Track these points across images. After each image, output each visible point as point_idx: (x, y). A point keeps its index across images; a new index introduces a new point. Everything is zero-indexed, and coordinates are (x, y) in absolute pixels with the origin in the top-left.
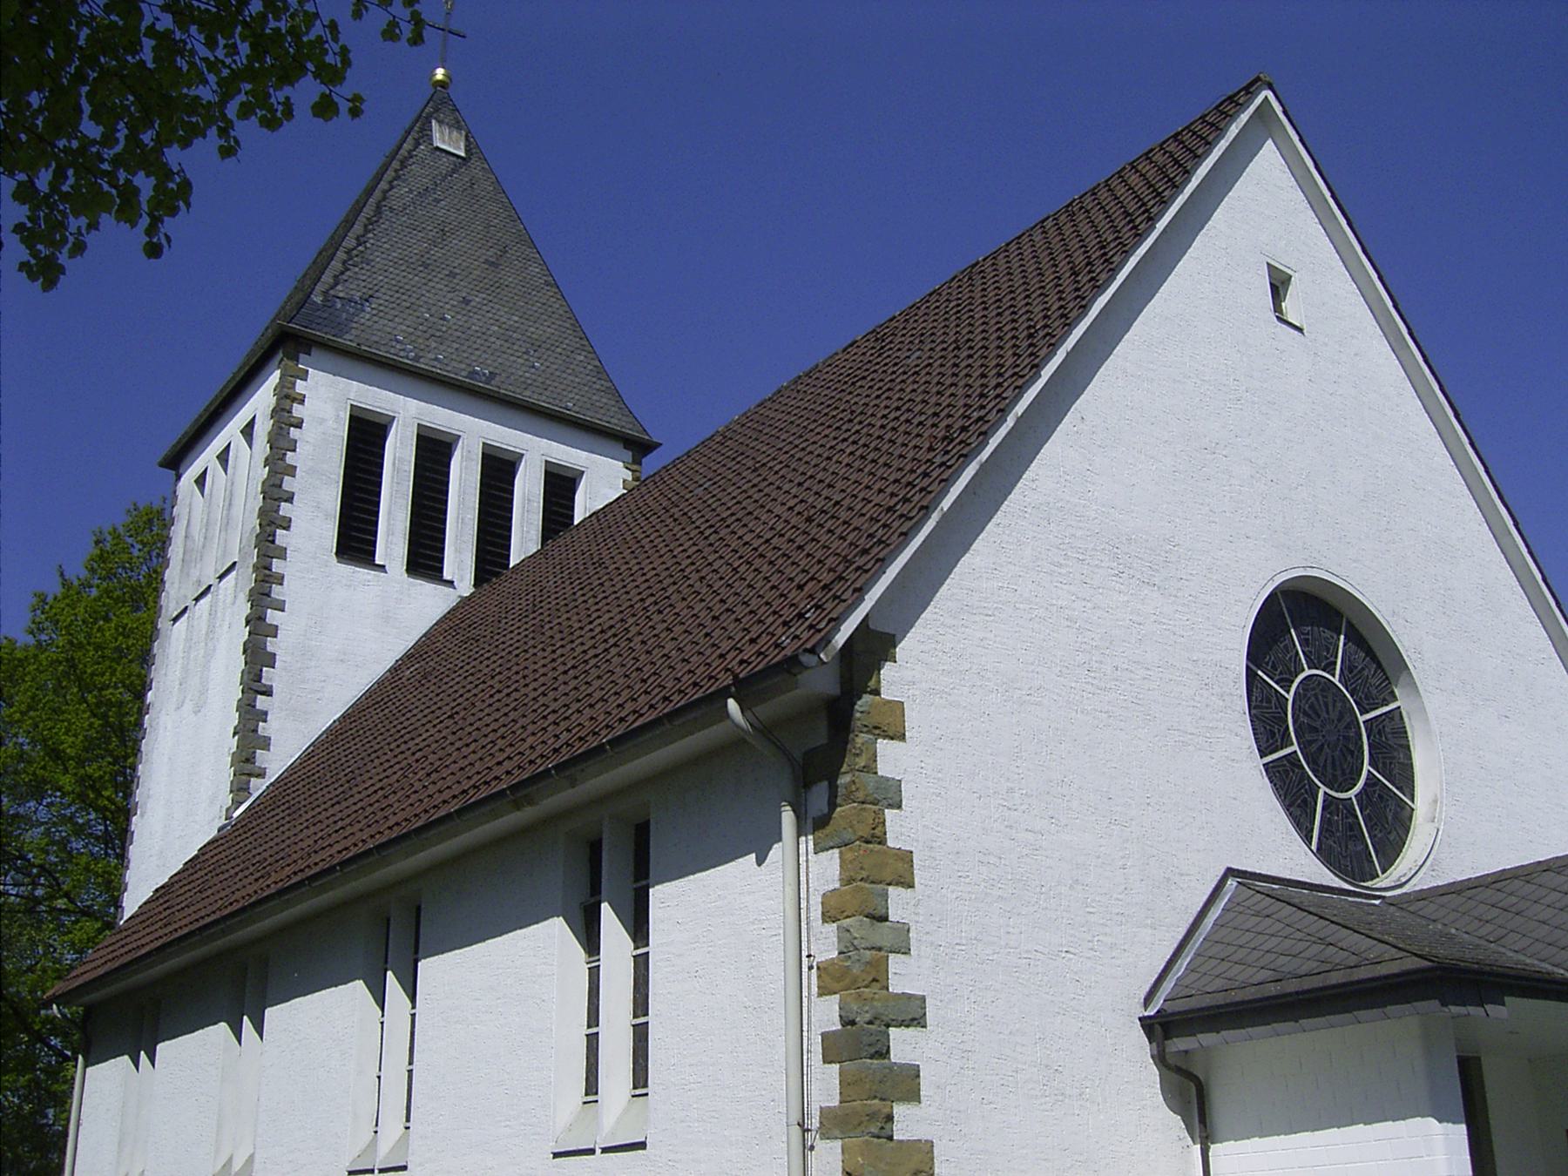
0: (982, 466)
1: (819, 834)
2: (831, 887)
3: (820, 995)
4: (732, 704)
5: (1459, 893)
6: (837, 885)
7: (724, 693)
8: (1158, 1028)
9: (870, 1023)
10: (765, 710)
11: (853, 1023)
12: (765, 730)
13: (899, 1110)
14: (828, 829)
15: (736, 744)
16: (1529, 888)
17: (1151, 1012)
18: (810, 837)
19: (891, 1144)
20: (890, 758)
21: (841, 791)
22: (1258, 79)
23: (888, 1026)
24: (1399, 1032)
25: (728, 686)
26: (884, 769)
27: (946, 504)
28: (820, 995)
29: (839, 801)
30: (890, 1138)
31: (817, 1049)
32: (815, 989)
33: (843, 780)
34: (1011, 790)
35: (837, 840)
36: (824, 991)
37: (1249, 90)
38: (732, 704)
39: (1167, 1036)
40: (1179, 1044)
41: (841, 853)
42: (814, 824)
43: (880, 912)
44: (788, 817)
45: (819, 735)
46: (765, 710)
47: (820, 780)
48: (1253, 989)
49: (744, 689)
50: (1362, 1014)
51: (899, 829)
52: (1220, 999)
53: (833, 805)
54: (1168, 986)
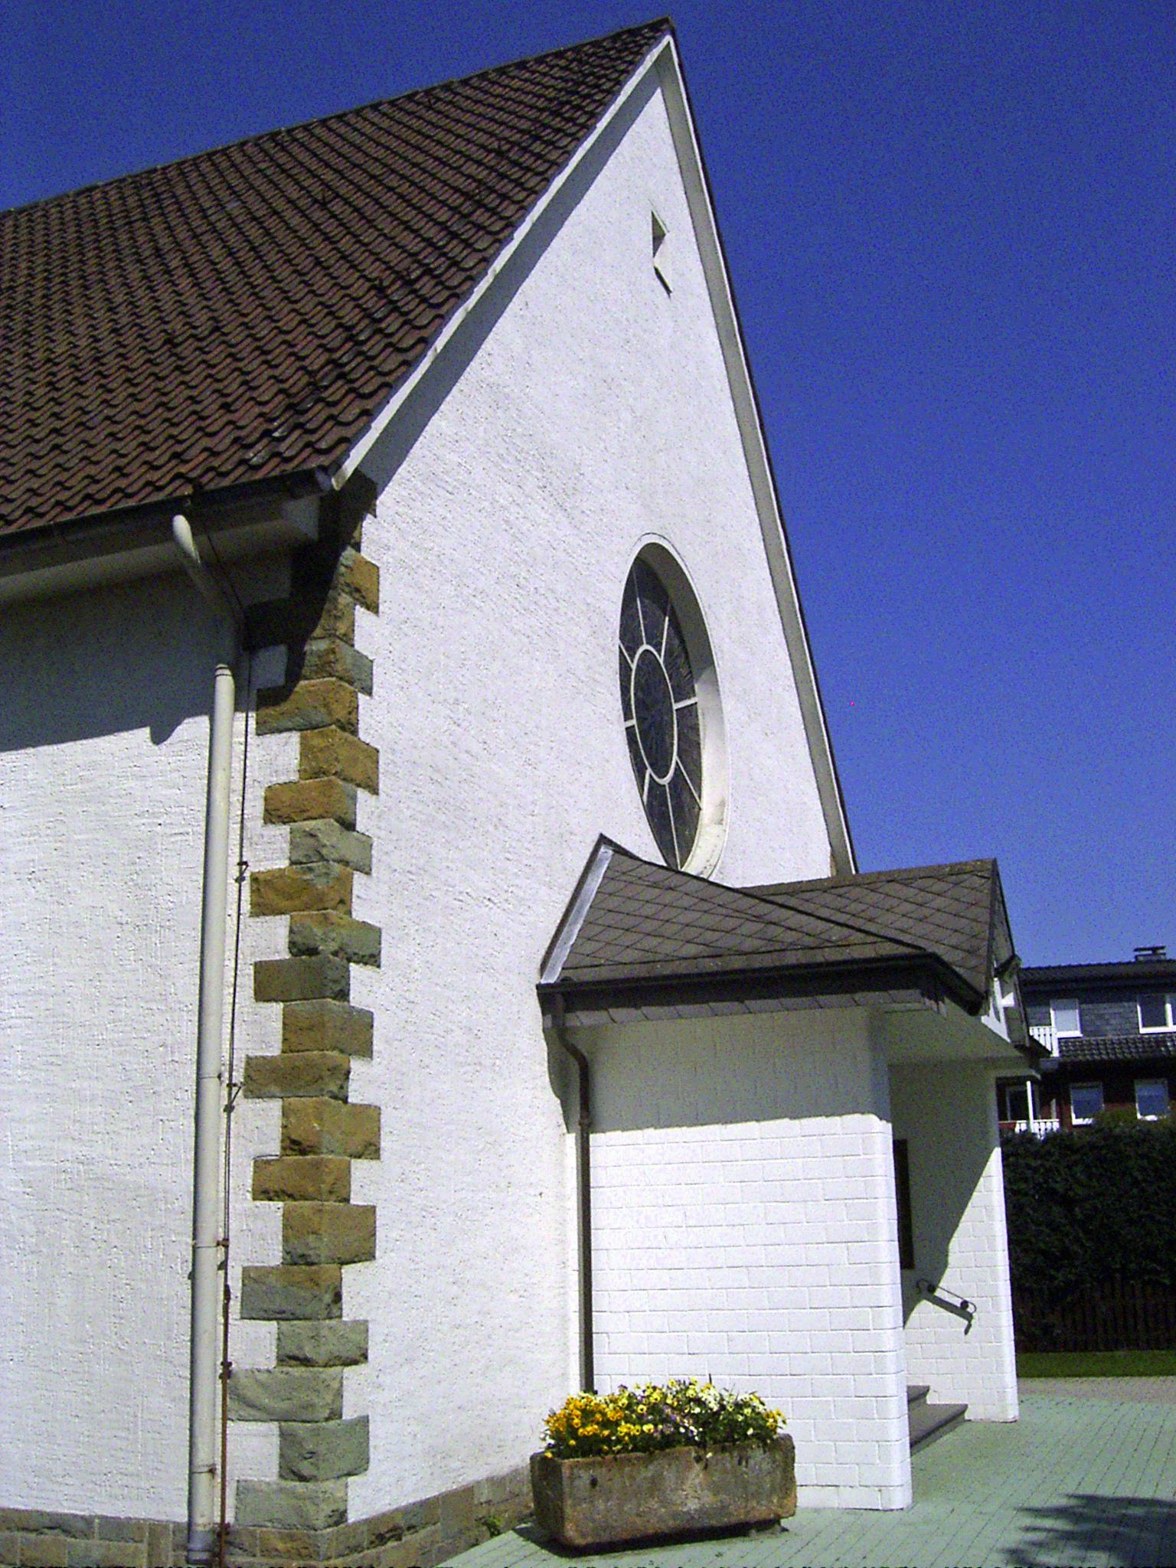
0: (469, 314)
1: (264, 711)
2: (283, 779)
3: (254, 914)
4: (181, 525)
5: (906, 883)
6: (294, 777)
7: (175, 506)
8: (559, 999)
9: (335, 954)
10: (231, 539)
11: (313, 951)
12: (215, 564)
13: (356, 1065)
14: (285, 707)
15: (173, 575)
16: (872, 897)
17: (552, 979)
18: (252, 715)
19: (345, 1109)
20: (369, 633)
21: (311, 660)
22: (666, 21)
23: (349, 960)
24: (843, 1019)
25: (183, 498)
26: (361, 644)
27: (440, 343)
28: (254, 914)
29: (305, 671)
30: (345, 1100)
31: (247, 982)
32: (246, 907)
33: (316, 646)
34: (457, 702)
35: (299, 720)
36: (261, 909)
37: (657, 29)
38: (181, 525)
39: (568, 1009)
40: (583, 1019)
41: (303, 738)
42: (266, 701)
43: (348, 817)
44: (225, 685)
45: (278, 586)
46: (231, 539)
47: (275, 643)
48: (684, 963)
49: (204, 509)
50: (788, 1001)
51: (375, 720)
52: (641, 971)
53: (294, 674)
54: (562, 954)
